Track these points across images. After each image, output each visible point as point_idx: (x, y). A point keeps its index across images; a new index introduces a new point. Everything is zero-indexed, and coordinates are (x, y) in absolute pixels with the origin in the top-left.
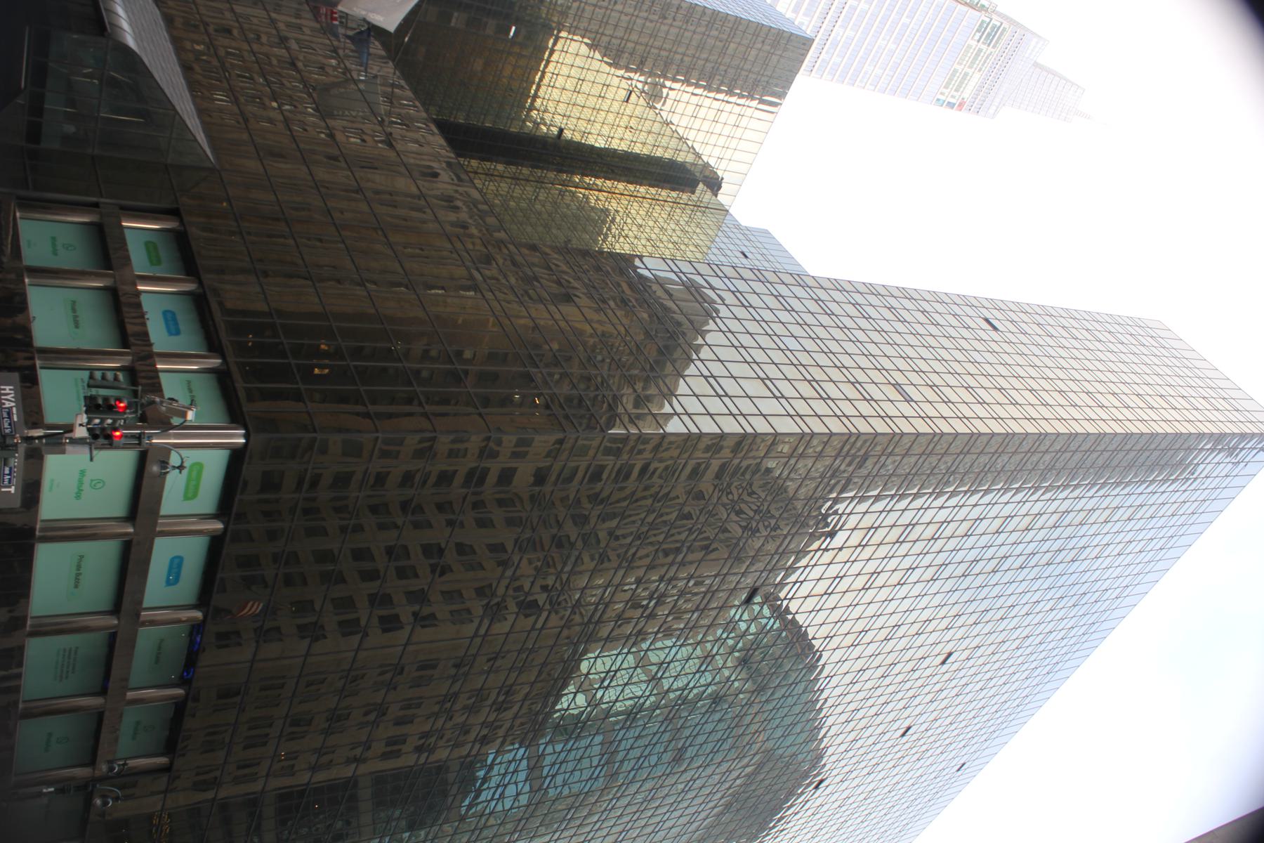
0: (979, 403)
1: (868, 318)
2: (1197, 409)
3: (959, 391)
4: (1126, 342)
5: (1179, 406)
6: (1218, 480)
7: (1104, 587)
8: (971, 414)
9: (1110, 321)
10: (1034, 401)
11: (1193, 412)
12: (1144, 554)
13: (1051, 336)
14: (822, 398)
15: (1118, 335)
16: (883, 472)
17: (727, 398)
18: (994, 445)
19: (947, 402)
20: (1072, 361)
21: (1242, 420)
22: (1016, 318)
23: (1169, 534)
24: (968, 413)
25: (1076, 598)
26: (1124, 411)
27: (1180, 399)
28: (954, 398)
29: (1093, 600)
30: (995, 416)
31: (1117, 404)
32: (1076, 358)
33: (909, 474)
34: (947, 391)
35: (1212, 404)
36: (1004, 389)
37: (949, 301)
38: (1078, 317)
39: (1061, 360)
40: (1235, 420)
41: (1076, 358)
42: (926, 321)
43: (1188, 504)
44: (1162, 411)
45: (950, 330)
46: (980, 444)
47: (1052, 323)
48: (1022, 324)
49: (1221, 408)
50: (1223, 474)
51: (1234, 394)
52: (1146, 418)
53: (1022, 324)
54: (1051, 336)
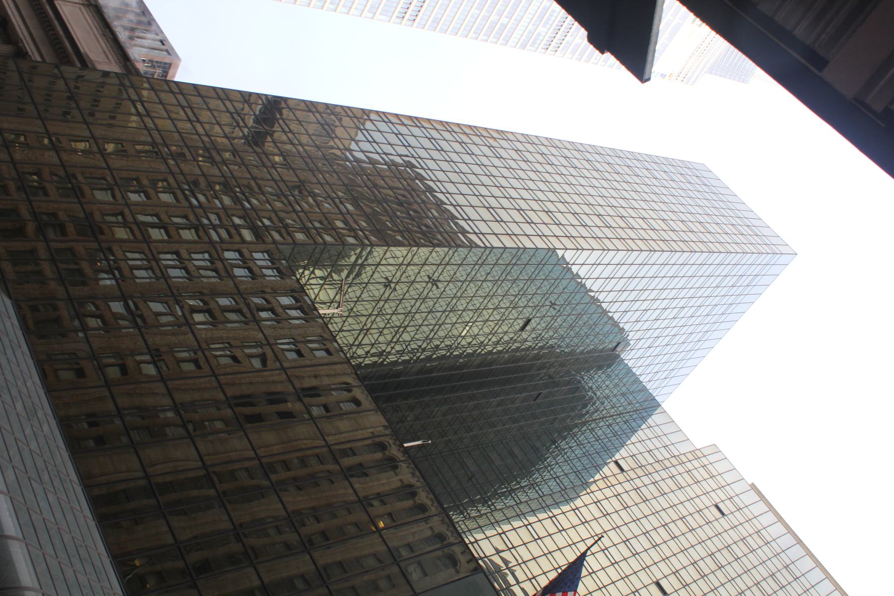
0: (528, 222)
1: (526, 161)
2: (757, 235)
3: (541, 214)
4: (693, 182)
5: (730, 232)
6: (741, 288)
7: (671, 368)
8: (519, 232)
9: (665, 163)
10: (600, 223)
11: (739, 236)
12: (686, 345)
13: (575, 168)
14: (556, 224)
15: (687, 176)
16: (509, 277)
17: (622, 226)
18: (507, 257)
19: (531, 223)
20: (633, 194)
21: (760, 242)
22: (591, 158)
23: (704, 330)
24: (575, 234)
25: (651, 375)
26: (671, 233)
27: (714, 225)
28: (564, 221)
29: (663, 377)
30: (540, 234)
31: (665, 228)
32: (636, 191)
33: (498, 280)
34: (531, 214)
35: (737, 230)
36: (523, 210)
37: (562, 146)
38: (622, 156)
39: (663, 197)
40: (754, 242)
41: (636, 191)
42: (544, 161)
43: (703, 308)
44: (717, 235)
45: (562, 169)
46: (525, 258)
47: (639, 166)
48: (616, 166)
49: (745, 233)
50: (745, 284)
51: (755, 222)
52: (687, 239)
53: (616, 166)
54: (575, 168)
